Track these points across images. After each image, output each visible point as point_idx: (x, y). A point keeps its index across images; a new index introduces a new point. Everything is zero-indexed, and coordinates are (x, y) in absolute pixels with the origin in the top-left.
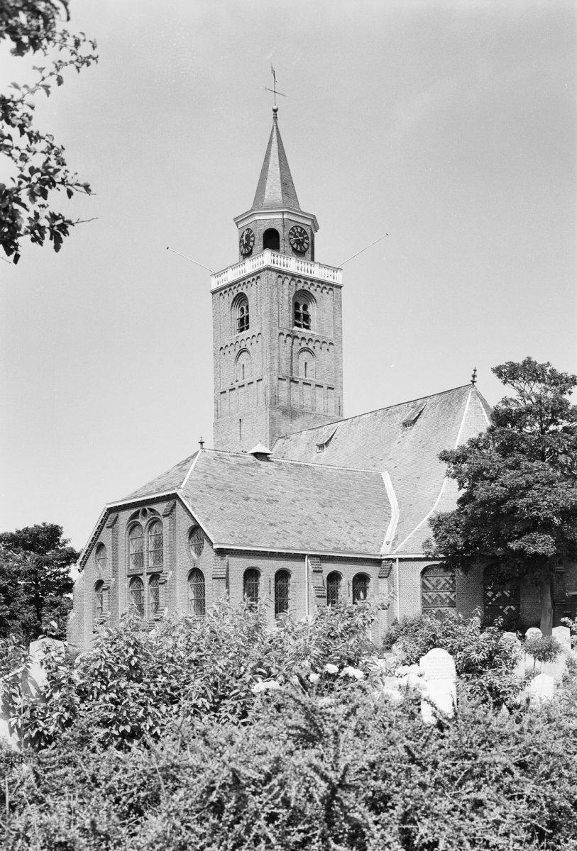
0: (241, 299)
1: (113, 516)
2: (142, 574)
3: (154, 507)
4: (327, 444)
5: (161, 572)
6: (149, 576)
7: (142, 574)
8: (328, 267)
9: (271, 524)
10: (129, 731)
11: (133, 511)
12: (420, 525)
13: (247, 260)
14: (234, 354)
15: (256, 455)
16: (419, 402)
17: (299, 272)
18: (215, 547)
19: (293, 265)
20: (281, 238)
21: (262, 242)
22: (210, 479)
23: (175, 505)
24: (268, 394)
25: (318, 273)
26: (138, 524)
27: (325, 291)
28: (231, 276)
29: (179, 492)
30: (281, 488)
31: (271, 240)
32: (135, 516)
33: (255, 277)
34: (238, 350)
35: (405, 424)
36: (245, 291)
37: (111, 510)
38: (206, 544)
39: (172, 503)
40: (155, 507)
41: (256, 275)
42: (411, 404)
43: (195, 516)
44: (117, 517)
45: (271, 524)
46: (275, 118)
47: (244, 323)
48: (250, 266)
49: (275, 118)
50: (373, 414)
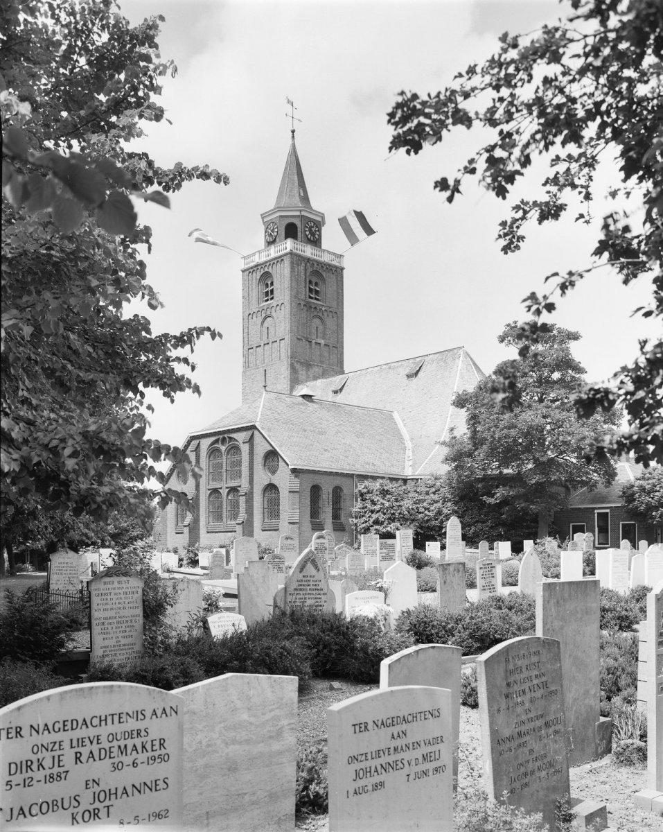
0: (267, 275)
1: (195, 443)
2: (221, 488)
3: (234, 435)
4: (341, 390)
5: (240, 486)
6: (227, 490)
7: (221, 488)
8: (334, 254)
9: (326, 450)
10: (633, 450)
11: (214, 439)
12: (432, 454)
13: (273, 247)
14: (260, 319)
15: (303, 396)
16: (418, 359)
17: (279, 254)
18: (290, 467)
19: (308, 251)
20: (299, 230)
21: (283, 233)
22: (276, 414)
23: (253, 434)
24: (289, 351)
25: (326, 258)
26: (218, 450)
27: (275, 266)
28: (257, 259)
29: (257, 425)
30: (326, 423)
31: (291, 231)
32: (216, 441)
33: (280, 260)
34: (264, 316)
35: (408, 376)
36: (270, 270)
37: (193, 438)
38: (281, 464)
39: (250, 433)
40: (234, 435)
41: (280, 259)
42: (411, 361)
43: (272, 443)
44: (199, 444)
45: (326, 450)
46: (293, 137)
47: (270, 294)
48: (274, 252)
49: (293, 137)
50: (379, 368)
